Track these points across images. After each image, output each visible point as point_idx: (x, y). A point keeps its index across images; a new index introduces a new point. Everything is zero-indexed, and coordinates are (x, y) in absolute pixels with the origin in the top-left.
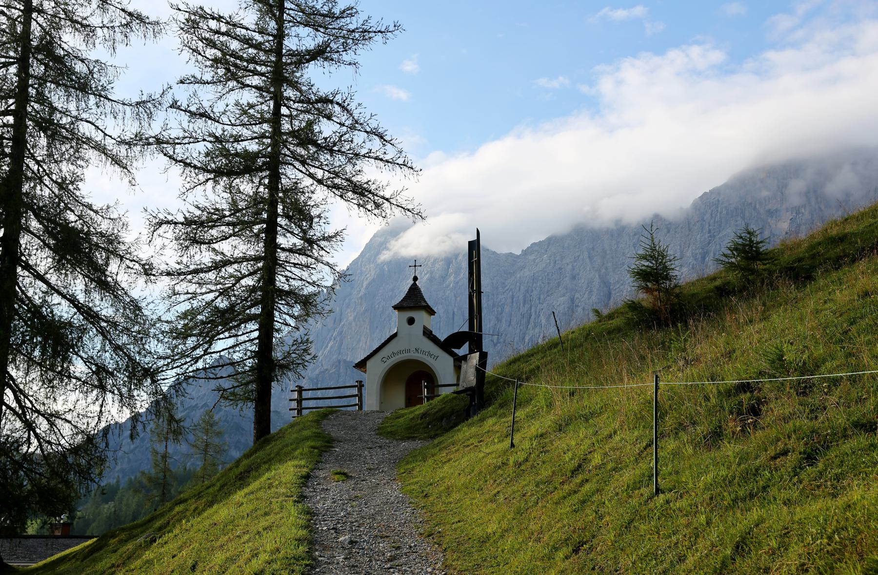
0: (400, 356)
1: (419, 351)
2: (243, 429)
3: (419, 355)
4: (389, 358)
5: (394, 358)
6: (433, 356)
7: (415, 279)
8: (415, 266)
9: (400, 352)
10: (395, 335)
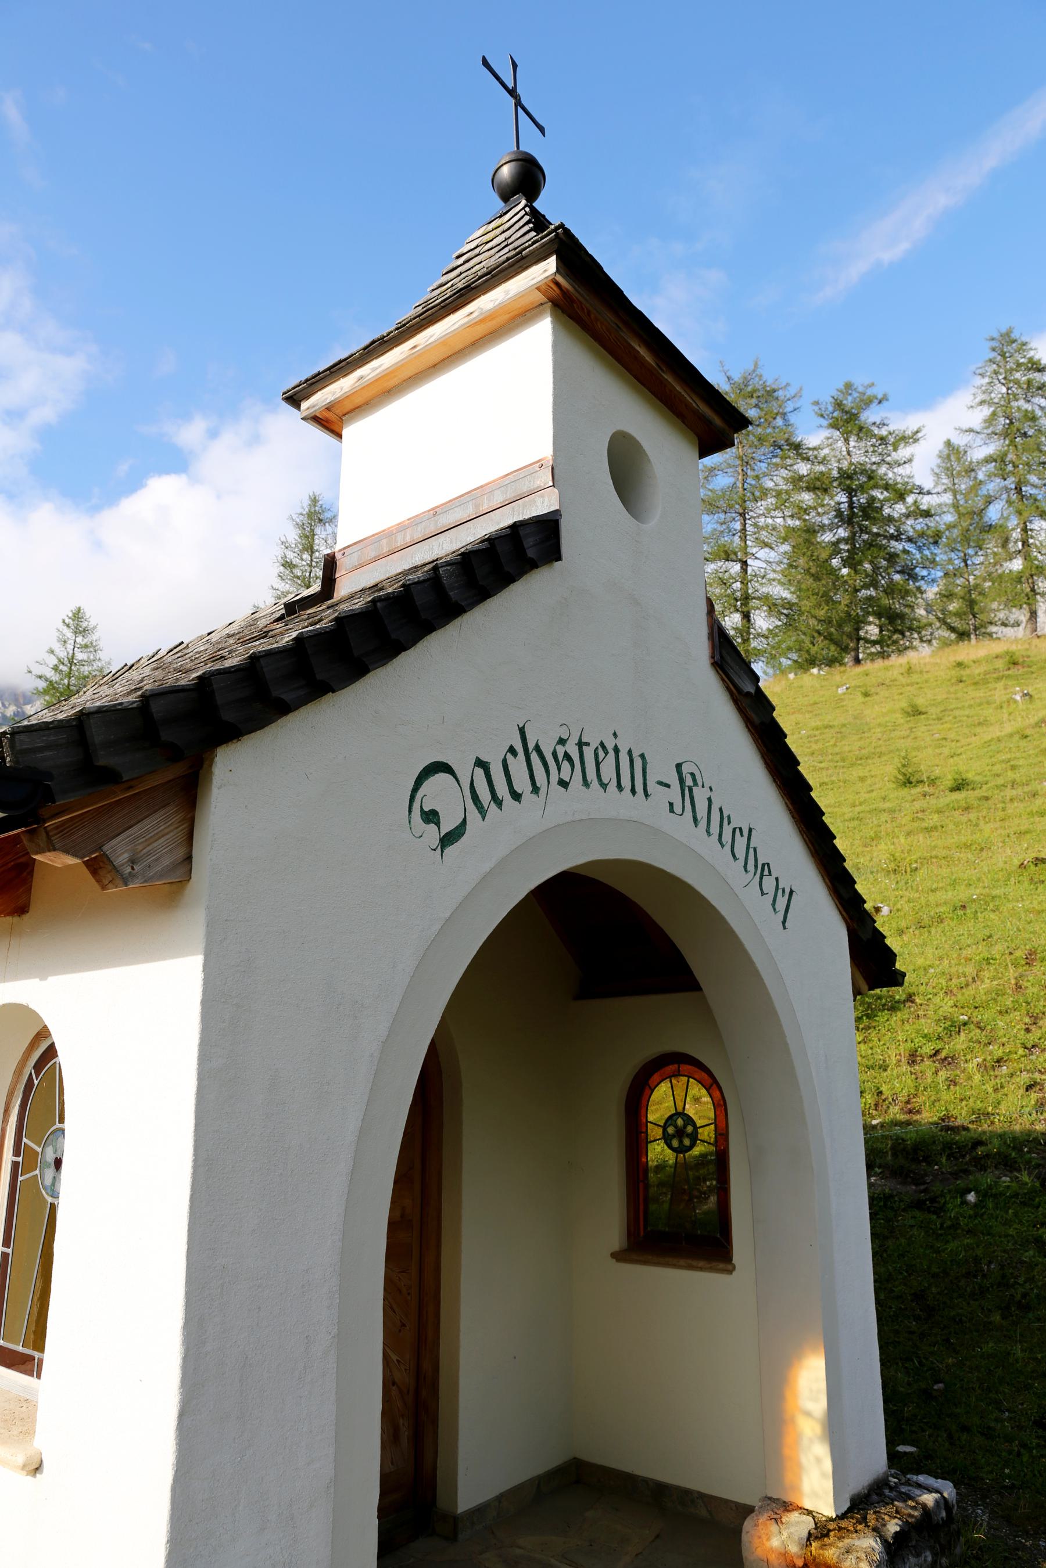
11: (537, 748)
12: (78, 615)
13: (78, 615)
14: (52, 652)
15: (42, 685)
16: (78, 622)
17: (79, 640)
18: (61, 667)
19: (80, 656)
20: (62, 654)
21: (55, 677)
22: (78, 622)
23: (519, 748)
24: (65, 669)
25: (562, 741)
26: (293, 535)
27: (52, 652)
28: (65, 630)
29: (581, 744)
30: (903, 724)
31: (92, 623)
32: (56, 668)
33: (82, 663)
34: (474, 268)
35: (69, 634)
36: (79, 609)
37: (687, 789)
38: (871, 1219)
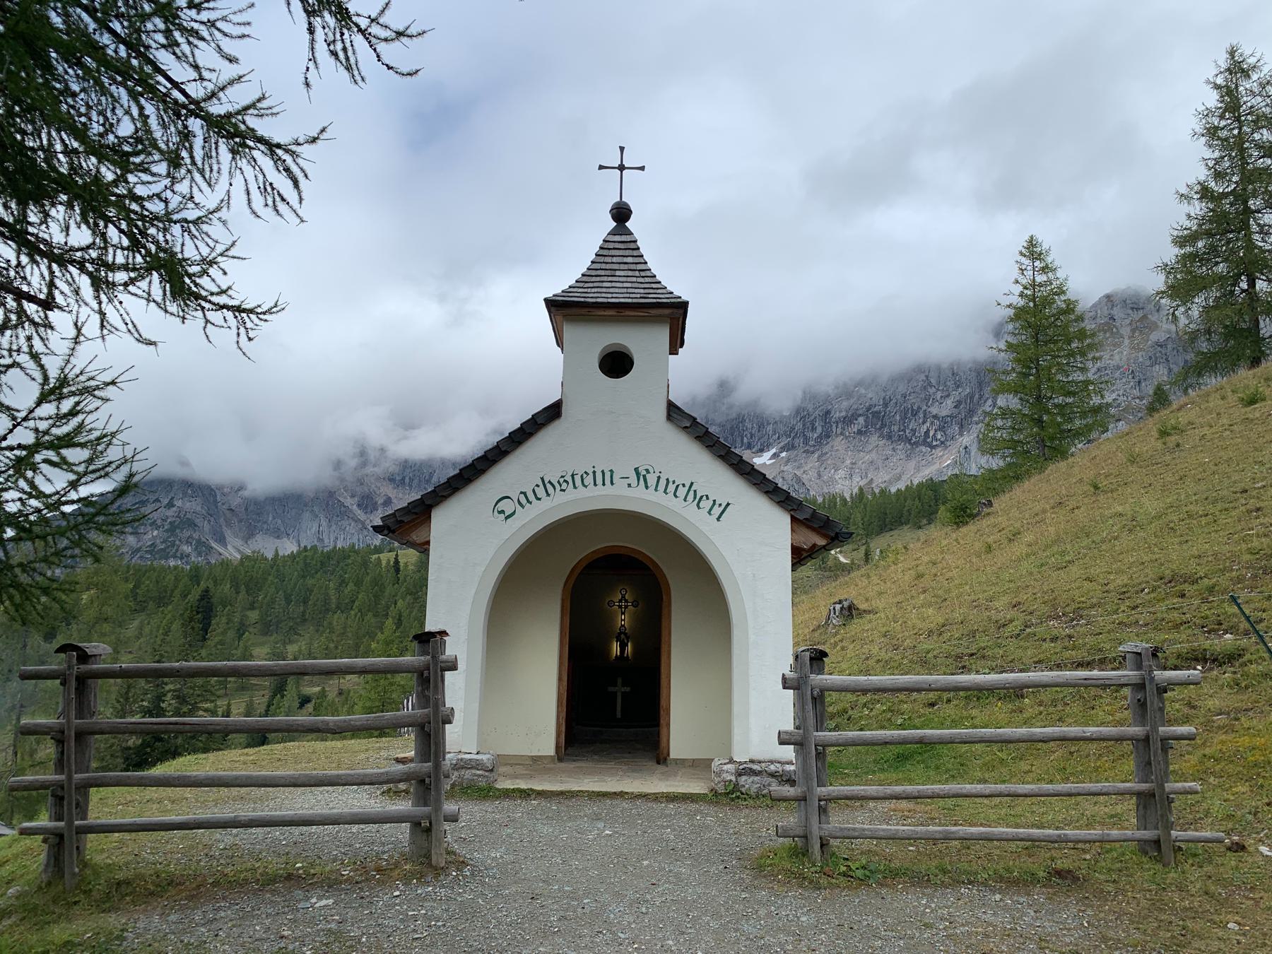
0: (571, 494)
1: (652, 479)
2: (196, 525)
3: (650, 495)
4: (525, 499)
5: (546, 503)
6: (706, 504)
7: (621, 213)
8: (622, 168)
9: (570, 481)
10: (553, 412)
11: (550, 482)
12: (1032, 243)
13: (1032, 243)
14: (1017, 282)
15: (1011, 312)
16: (1033, 250)
17: (1037, 263)
18: (1026, 292)
19: (1040, 278)
20: (1024, 282)
21: (1021, 302)
22: (1033, 250)
23: (540, 484)
24: (1029, 292)
25: (562, 477)
26: (1212, 99)
27: (1017, 282)
28: (1024, 260)
29: (573, 476)
30: (5, 608)
31: (1045, 246)
32: (1021, 295)
33: (1040, 285)
34: (638, 265)
35: (1026, 261)
36: (1032, 237)
37: (641, 477)
38: (427, 579)
